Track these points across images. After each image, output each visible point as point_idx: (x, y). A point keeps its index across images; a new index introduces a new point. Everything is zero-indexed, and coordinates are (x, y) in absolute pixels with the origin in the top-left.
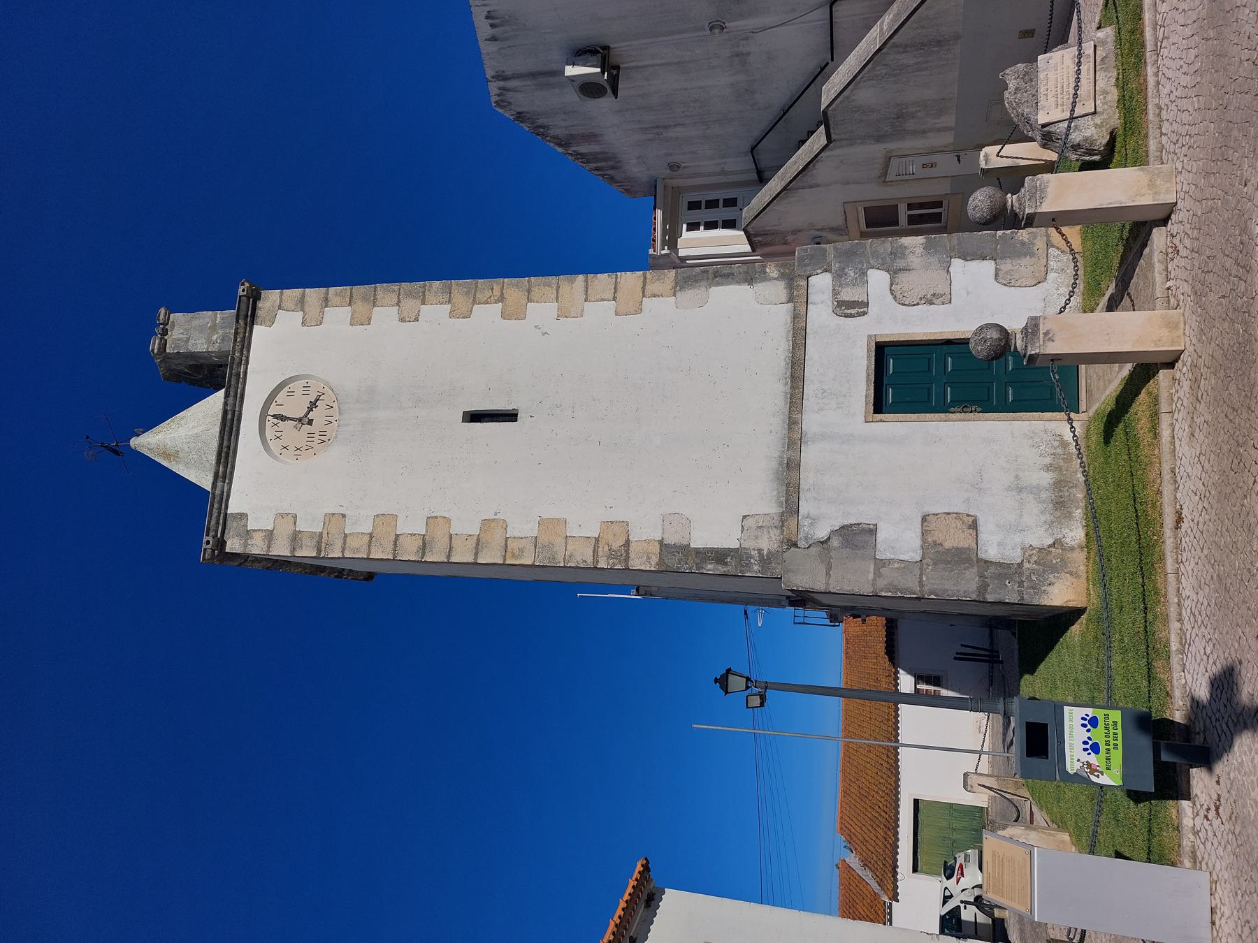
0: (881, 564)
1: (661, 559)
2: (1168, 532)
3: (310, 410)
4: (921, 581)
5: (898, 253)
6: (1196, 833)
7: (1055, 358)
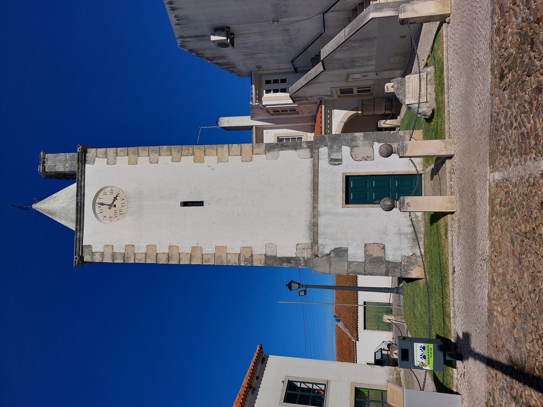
0: (350, 263)
1: (265, 262)
2: (450, 275)
3: (114, 201)
4: (365, 269)
5: (353, 139)
6: (458, 380)
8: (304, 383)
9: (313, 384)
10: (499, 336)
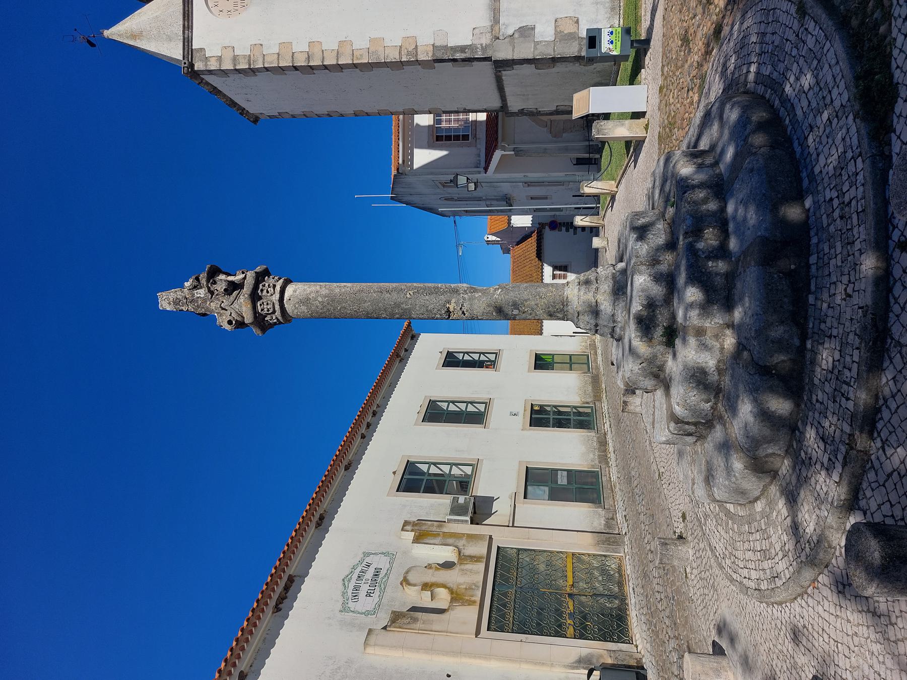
0: (537, 43)
8: (467, 353)
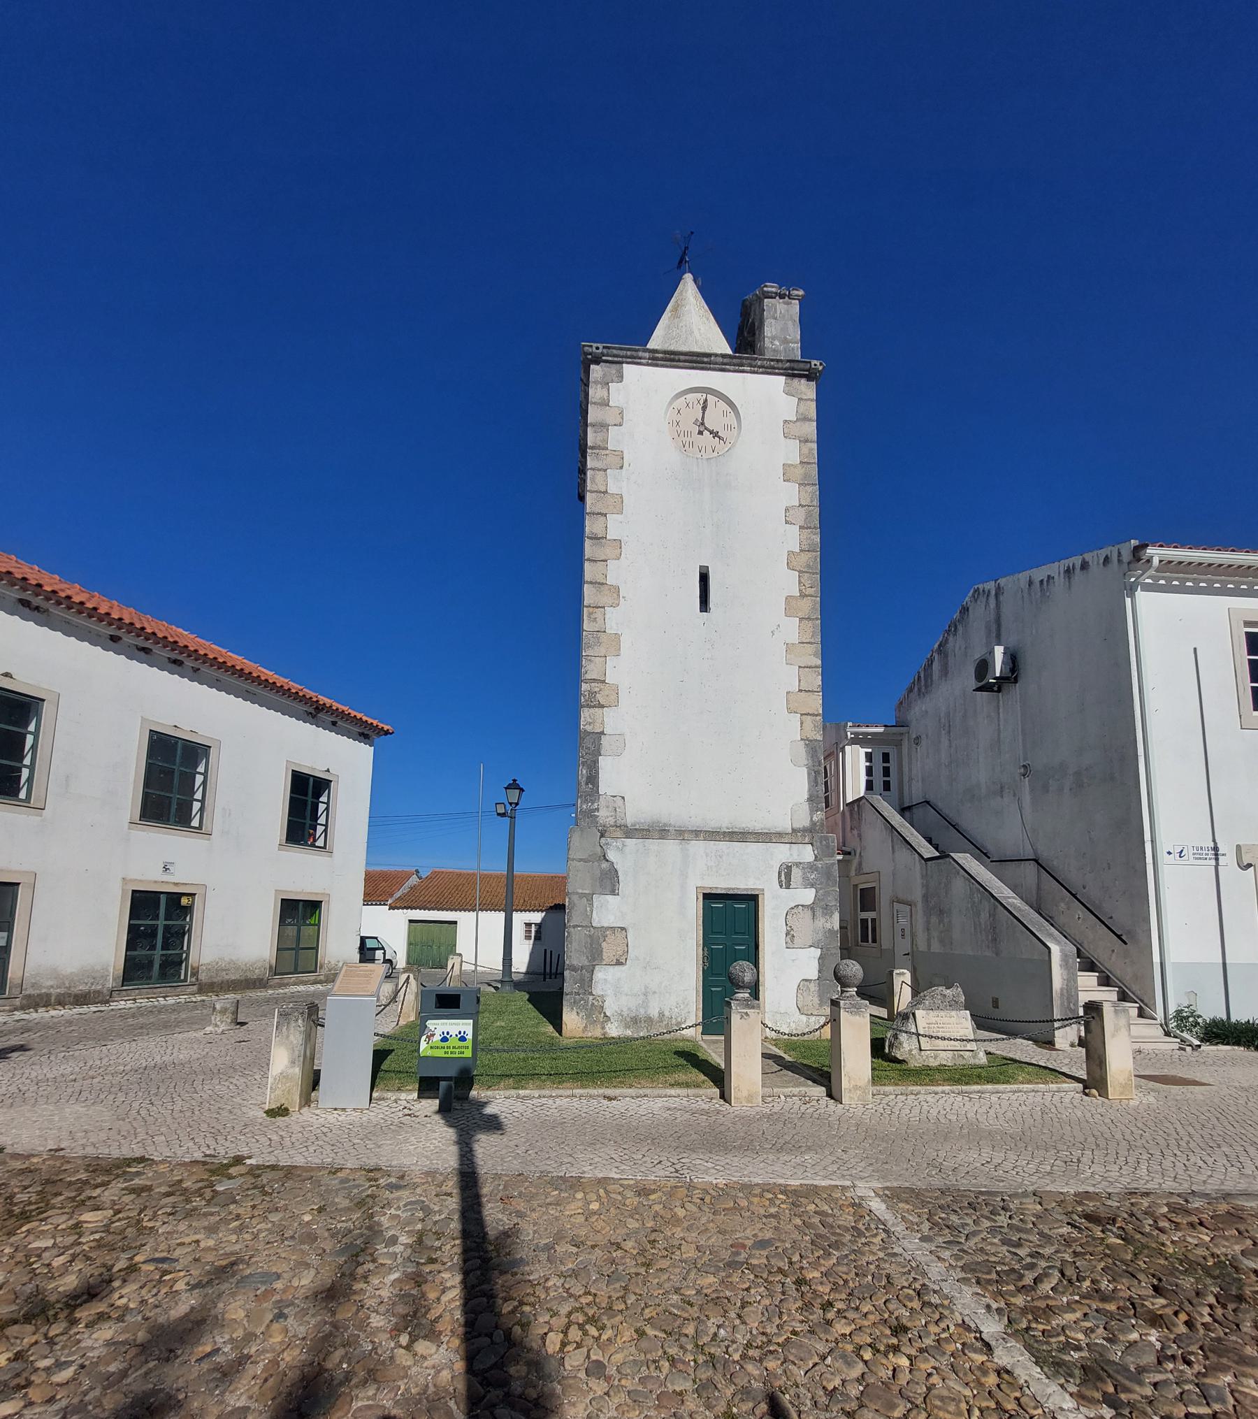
0: (590, 898)
2: (601, 1091)
5: (827, 911)
7: (729, 1019)
8: (327, 809)
9: (326, 825)
10: (535, 1203)
